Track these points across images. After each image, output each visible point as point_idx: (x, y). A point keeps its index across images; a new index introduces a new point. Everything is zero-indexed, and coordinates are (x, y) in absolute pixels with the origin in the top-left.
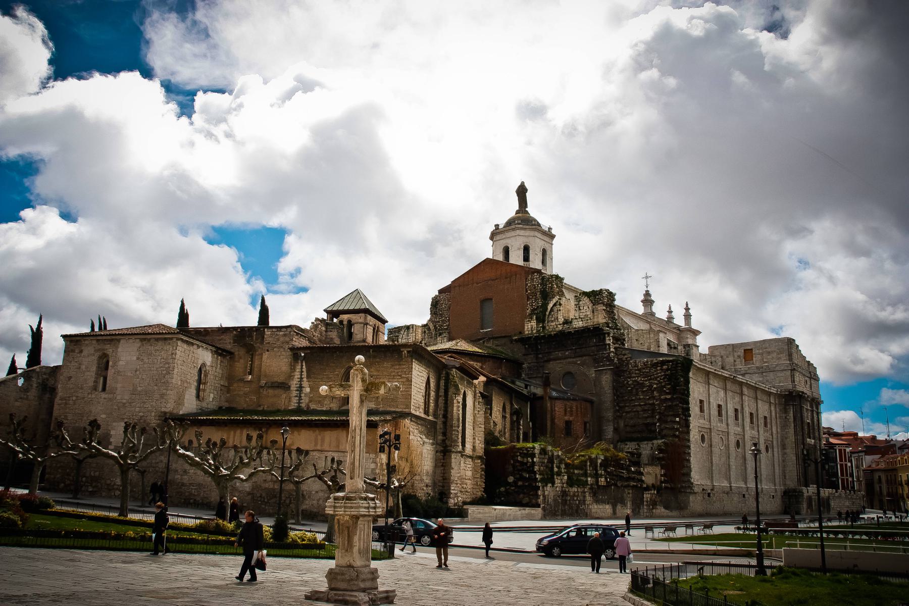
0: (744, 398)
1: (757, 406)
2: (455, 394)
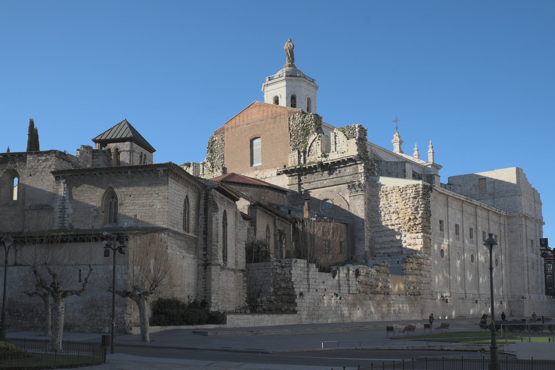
0: (478, 219)
1: (489, 226)
2: (214, 212)
